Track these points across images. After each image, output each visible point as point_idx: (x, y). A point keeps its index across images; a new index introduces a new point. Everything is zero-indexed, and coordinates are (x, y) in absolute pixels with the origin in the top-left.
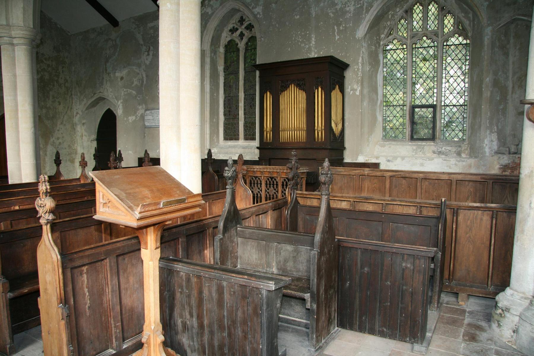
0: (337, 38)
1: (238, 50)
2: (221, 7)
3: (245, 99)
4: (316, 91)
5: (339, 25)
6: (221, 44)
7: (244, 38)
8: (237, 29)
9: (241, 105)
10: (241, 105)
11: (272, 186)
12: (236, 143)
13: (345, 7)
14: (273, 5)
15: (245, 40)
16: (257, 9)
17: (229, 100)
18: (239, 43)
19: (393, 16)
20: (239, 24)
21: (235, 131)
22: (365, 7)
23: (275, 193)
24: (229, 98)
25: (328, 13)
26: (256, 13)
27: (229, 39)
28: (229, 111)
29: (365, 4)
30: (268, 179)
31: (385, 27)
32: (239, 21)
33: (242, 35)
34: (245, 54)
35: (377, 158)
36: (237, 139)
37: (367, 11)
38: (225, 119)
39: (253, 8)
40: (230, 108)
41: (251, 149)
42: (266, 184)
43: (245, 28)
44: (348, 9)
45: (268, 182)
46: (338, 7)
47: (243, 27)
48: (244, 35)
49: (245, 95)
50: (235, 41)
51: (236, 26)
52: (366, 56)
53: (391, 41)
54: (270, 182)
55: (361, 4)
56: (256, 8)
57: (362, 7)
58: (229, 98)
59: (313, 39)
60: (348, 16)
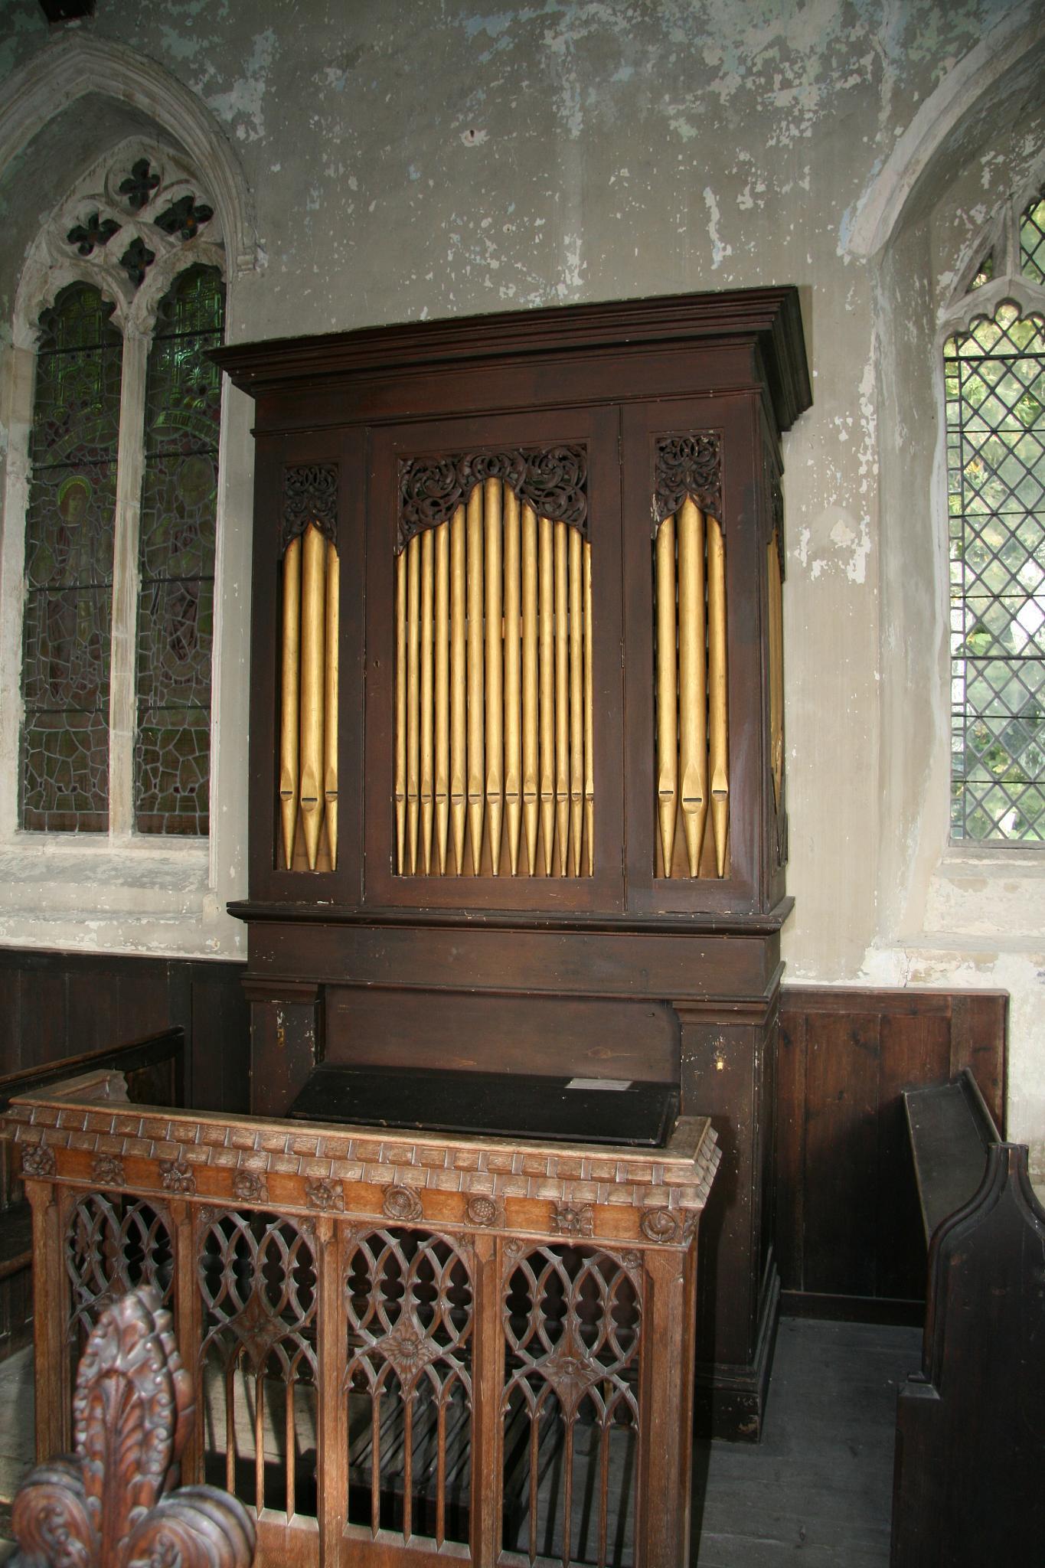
0: (718, 257)
1: (115, 338)
2: (20, 77)
3: (143, 601)
4: (666, 528)
5: (730, 184)
6: (20, 303)
7: (151, 272)
8: (112, 228)
9: (124, 634)
10: (124, 634)
11: (410, 1301)
12: (89, 852)
13: (768, 87)
14: (333, 73)
15: (155, 284)
16: (233, 97)
17: (53, 608)
18: (121, 297)
19: (1001, 175)
20: (125, 200)
21: (83, 780)
22: (886, 89)
23: (441, 1365)
24: (53, 598)
25: (664, 120)
26: (229, 116)
27: (64, 278)
28: (54, 671)
29: (890, 73)
30: (376, 1243)
31: (958, 235)
32: (126, 187)
33: (138, 259)
34: (153, 358)
35: (983, 962)
36: (97, 825)
37: (905, 111)
38: (30, 713)
39: (210, 89)
40: (58, 651)
41: (178, 887)
42: (359, 1284)
43: (158, 221)
44: (782, 99)
45: (376, 1273)
46: (725, 88)
47: (149, 215)
48: (149, 258)
49: (146, 583)
50: (96, 291)
51: (107, 213)
52: (889, 365)
53: (990, 310)
54: (392, 1267)
55: (860, 71)
56: (227, 88)
57: (869, 90)
58: (53, 598)
59: (574, 259)
60: (786, 135)
